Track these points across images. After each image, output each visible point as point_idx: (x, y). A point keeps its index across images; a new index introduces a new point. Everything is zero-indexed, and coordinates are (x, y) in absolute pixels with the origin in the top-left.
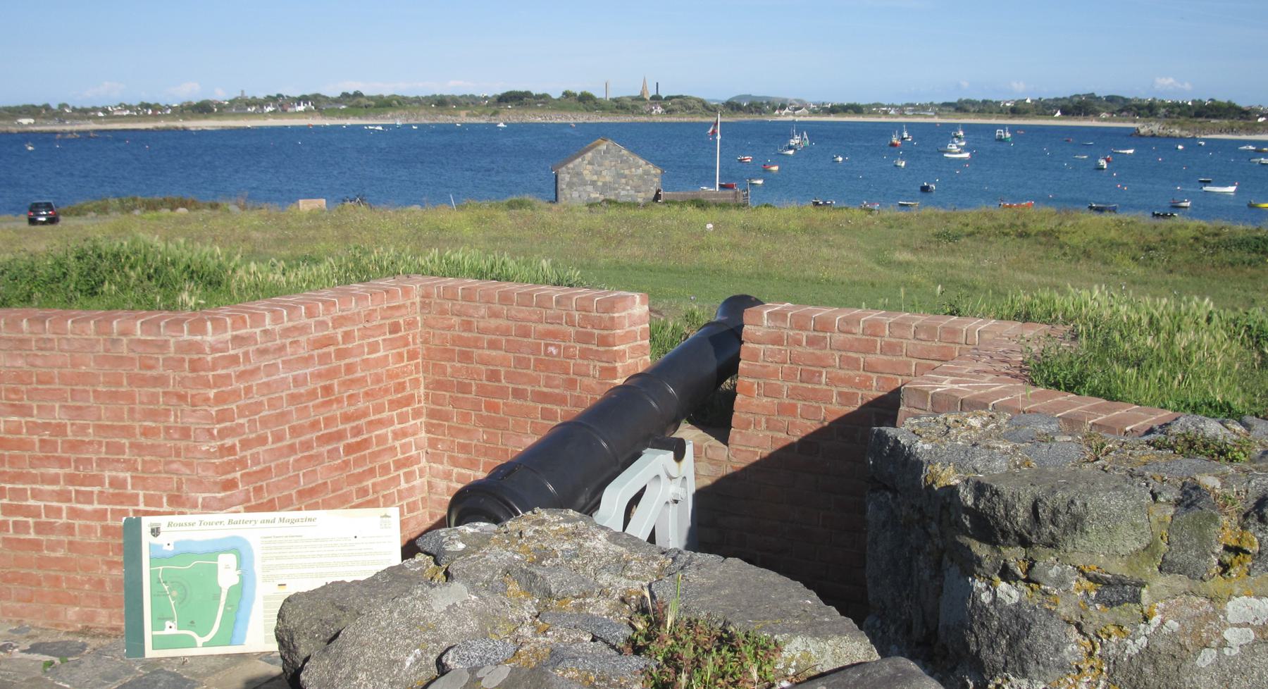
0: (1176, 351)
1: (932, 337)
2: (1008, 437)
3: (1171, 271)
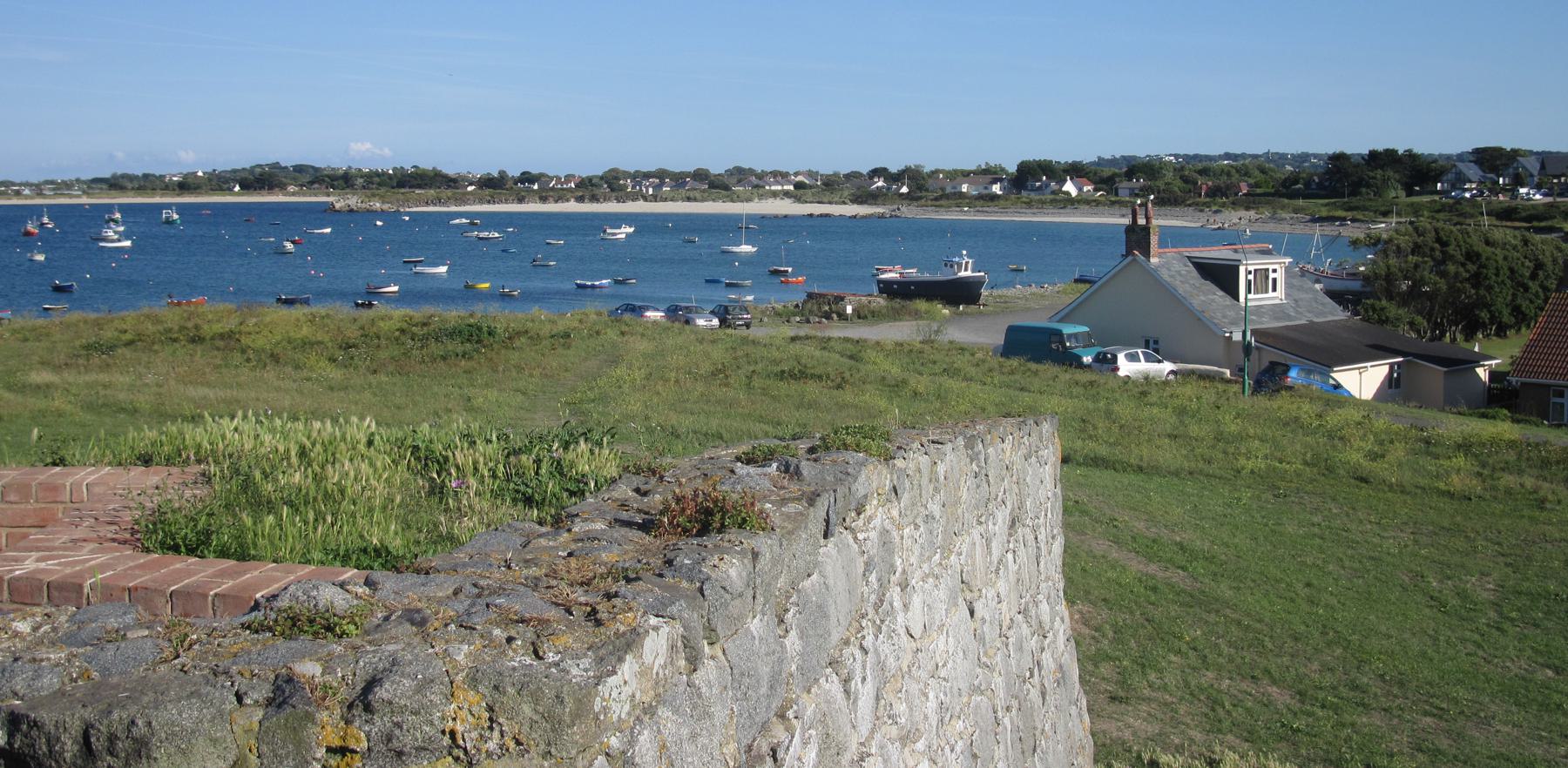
0: (329, 487)
1: (26, 497)
2: (70, 640)
3: (375, 372)
